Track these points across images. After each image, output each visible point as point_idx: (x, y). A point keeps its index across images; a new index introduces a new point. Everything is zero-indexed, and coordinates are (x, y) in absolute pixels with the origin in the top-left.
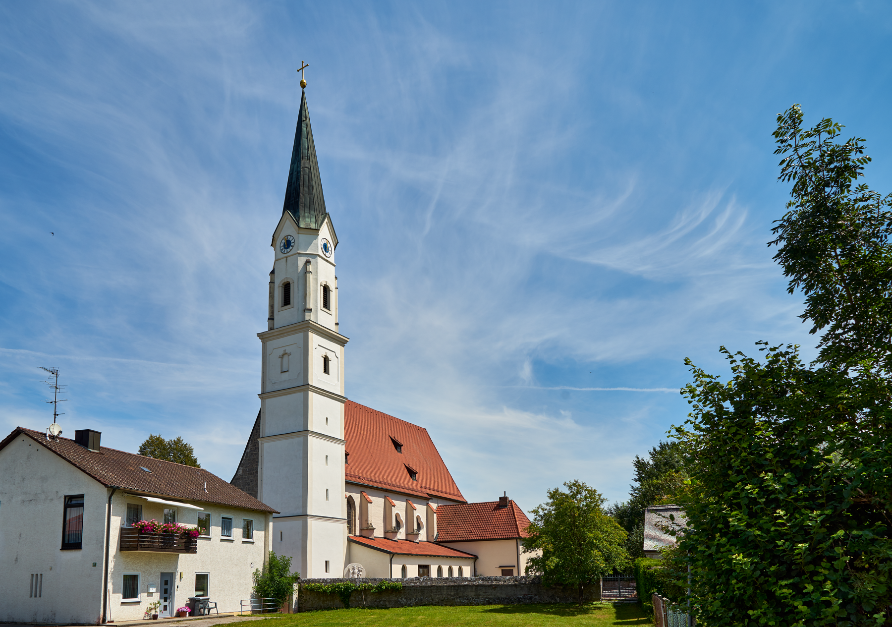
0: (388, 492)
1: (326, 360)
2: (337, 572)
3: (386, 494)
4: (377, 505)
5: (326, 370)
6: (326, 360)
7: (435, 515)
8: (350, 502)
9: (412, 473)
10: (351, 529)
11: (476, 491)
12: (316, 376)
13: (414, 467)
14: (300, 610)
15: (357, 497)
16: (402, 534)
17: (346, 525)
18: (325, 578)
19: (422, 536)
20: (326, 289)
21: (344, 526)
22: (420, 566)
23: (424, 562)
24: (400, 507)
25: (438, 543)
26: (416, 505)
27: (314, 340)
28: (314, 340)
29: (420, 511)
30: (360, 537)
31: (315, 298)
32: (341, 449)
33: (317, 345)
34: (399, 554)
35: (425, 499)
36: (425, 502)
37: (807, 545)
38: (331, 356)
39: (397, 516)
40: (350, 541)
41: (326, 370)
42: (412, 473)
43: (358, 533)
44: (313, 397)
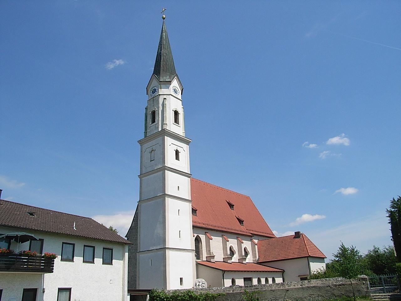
0: (224, 233)
1: (177, 152)
2: (188, 285)
3: (223, 234)
4: (216, 243)
5: (177, 158)
6: (177, 152)
7: (256, 246)
8: (198, 240)
9: (241, 222)
10: (198, 256)
11: (281, 230)
12: (170, 161)
13: (242, 218)
14: (196, 261)
15: (203, 237)
16: (235, 258)
17: (194, 254)
18: (180, 289)
19: (249, 259)
20: (176, 113)
21: (192, 255)
22: (245, 279)
23: (248, 276)
24: (233, 243)
25: (260, 263)
26: (243, 241)
27: (168, 141)
28: (168, 141)
29: (247, 244)
30: (203, 265)
31: (170, 117)
32: (188, 207)
33: (170, 145)
34: (228, 271)
35: (250, 237)
36: (249, 238)
37: (396, 256)
38: (179, 149)
39: (231, 248)
40: (198, 264)
41: (177, 158)
42: (241, 222)
43: (205, 259)
44: (168, 174)
